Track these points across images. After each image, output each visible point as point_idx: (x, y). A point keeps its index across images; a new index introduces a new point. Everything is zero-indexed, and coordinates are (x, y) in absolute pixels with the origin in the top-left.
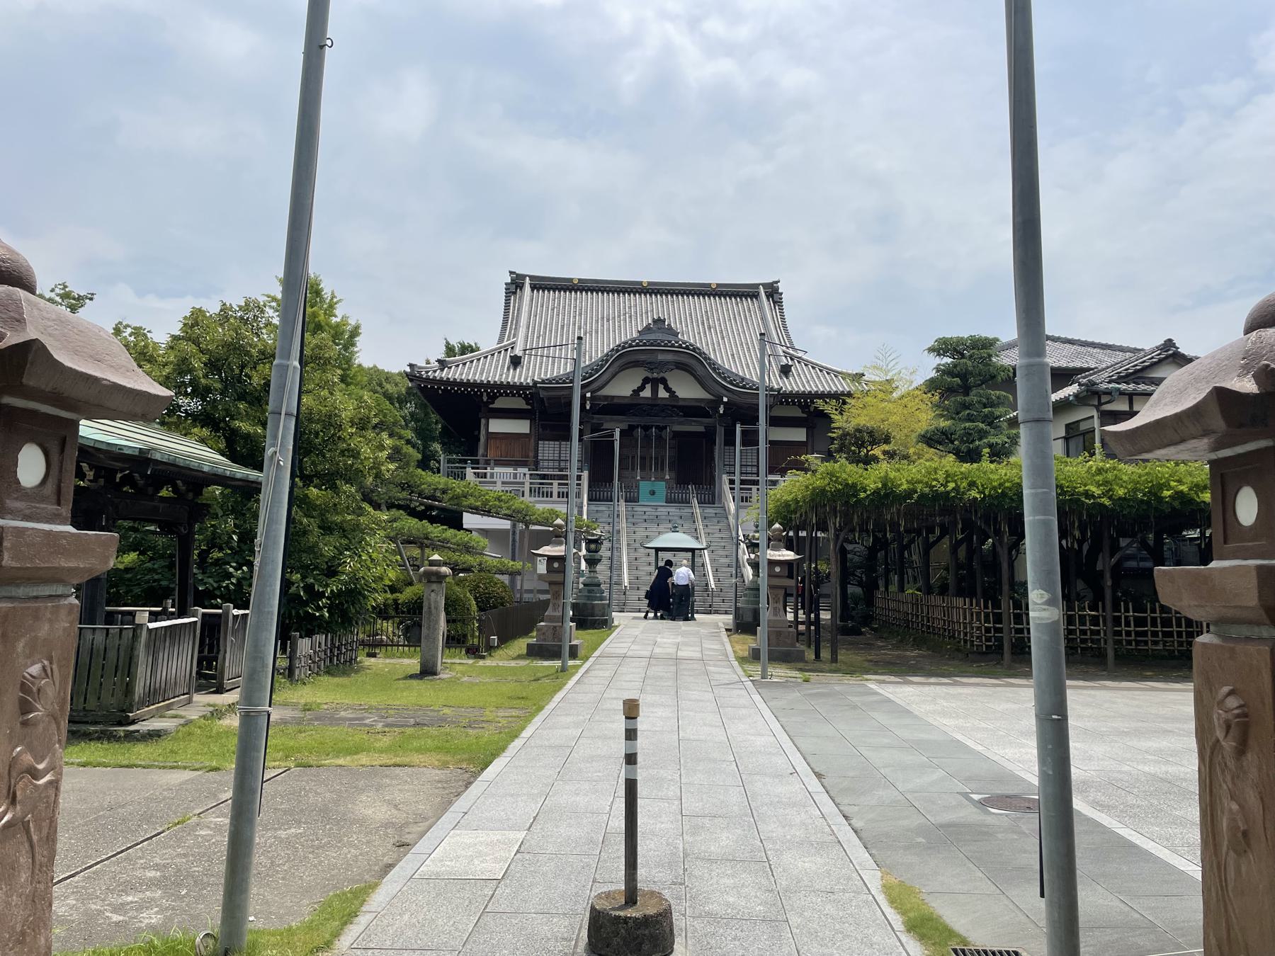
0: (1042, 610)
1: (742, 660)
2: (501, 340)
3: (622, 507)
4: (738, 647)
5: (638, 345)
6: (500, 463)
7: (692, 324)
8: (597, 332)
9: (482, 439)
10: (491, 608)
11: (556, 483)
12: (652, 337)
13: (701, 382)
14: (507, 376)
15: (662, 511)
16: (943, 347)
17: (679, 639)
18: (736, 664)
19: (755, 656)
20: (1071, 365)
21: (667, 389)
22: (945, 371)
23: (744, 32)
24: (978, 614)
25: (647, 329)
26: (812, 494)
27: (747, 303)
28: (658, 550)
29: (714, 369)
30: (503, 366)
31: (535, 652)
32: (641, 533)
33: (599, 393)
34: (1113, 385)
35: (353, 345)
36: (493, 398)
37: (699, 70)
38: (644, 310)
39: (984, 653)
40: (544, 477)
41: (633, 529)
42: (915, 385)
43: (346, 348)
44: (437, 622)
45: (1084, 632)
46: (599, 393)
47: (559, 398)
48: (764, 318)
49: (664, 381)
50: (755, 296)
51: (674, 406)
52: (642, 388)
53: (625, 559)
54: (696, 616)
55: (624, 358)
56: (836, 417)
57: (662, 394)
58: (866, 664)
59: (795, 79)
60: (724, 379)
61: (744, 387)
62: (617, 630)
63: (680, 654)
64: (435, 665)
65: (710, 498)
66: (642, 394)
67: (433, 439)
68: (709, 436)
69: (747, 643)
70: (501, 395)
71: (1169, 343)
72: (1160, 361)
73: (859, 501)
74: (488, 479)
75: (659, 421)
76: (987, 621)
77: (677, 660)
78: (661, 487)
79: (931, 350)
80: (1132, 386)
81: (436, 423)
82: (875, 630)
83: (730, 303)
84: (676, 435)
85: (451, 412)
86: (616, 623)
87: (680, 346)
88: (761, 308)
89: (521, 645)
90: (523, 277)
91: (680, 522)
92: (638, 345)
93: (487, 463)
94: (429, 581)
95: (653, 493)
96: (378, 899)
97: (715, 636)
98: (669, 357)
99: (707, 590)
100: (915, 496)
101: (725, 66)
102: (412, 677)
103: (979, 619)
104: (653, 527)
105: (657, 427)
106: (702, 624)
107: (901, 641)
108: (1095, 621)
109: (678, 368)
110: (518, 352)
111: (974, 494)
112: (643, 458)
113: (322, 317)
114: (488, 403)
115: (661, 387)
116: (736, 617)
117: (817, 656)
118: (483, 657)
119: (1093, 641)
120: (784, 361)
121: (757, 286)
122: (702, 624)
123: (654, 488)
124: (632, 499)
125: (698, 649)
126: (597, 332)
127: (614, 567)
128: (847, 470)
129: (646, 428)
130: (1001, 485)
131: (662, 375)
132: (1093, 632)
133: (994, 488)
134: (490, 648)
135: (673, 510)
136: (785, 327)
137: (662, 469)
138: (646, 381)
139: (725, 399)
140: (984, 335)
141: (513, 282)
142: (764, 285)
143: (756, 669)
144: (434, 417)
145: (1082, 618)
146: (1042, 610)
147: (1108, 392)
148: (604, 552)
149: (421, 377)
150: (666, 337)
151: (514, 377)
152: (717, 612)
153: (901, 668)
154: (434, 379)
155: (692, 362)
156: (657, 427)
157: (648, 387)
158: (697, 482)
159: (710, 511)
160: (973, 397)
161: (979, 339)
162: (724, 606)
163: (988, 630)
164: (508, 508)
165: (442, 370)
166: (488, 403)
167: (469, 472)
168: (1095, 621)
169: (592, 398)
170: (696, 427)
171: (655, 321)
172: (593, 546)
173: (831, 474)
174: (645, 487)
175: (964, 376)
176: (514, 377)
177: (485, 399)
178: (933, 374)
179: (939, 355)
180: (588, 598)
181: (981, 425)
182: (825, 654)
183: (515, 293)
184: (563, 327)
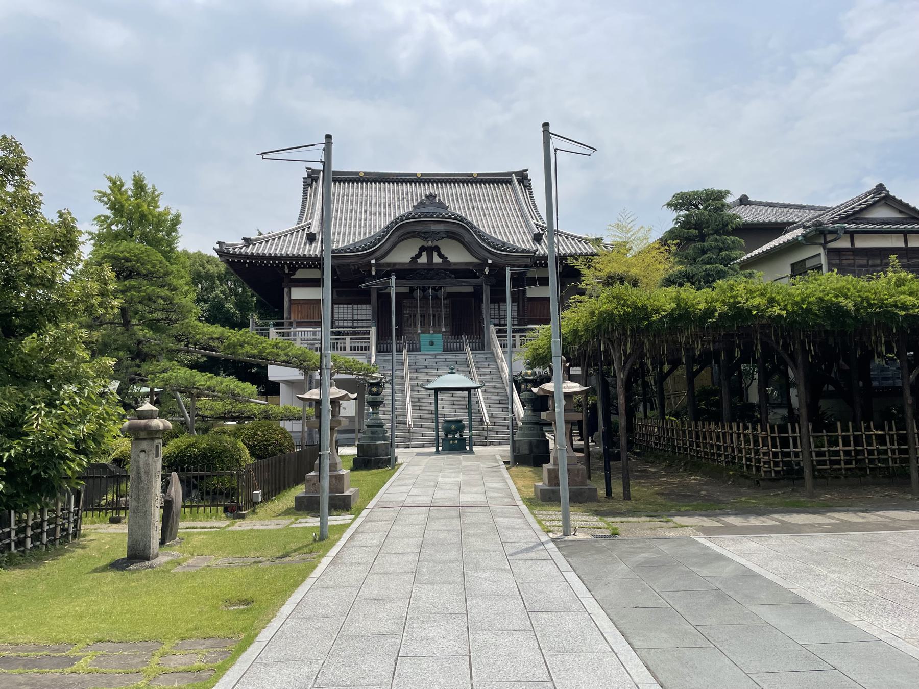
0: (852, 439)
1: (531, 503)
2: (300, 221)
3: (405, 355)
4: (520, 483)
5: (413, 218)
6: (300, 324)
7: (456, 201)
8: (380, 214)
9: (286, 305)
10: (270, 455)
11: (348, 338)
12: (425, 210)
14: (304, 250)
15: (440, 358)
16: (682, 201)
17: (460, 478)
18: (525, 509)
19: (548, 497)
20: (779, 220)
21: (440, 255)
22: (686, 224)
23: (485, 21)
24: (765, 439)
25: (421, 204)
26: (599, 319)
27: (503, 188)
28: (437, 390)
29: (479, 236)
30: (300, 243)
31: (307, 506)
32: (422, 377)
33: (384, 261)
34: (836, 225)
35: (175, 230)
36: (293, 270)
37: (453, 48)
38: (419, 192)
39: (771, 480)
40: (339, 333)
41: (416, 374)
42: (651, 241)
43: (169, 234)
44: (148, 490)
45: (871, 452)
46: (384, 261)
47: (348, 265)
48: (517, 199)
49: (437, 249)
50: (509, 182)
51: (445, 270)
52: (419, 255)
53: (408, 400)
54: (474, 448)
55: (403, 230)
56: (584, 271)
57: (437, 259)
58: (660, 499)
59: (523, 53)
60: (488, 244)
61: (505, 250)
62: (400, 470)
63: (465, 498)
64: (147, 546)
65: (481, 345)
66: (419, 261)
67: (250, 309)
68: (477, 295)
69: (533, 480)
70: (300, 267)
71: (880, 188)
72: (875, 203)
73: (650, 324)
74: (292, 337)
75: (433, 283)
76: (774, 446)
77: (460, 509)
78: (439, 338)
79: (669, 205)
80: (853, 226)
81: (253, 296)
82: (638, 454)
83: (489, 188)
84: (449, 295)
85: (262, 281)
86: (399, 461)
87: (450, 218)
88: (515, 192)
89: (288, 499)
91: (457, 366)
92: (413, 218)
93: (291, 324)
94: (137, 439)
95: (432, 344)
97: (495, 470)
98: (441, 227)
99: (482, 424)
100: (716, 314)
101: (473, 45)
102: (118, 565)
103: (765, 444)
104: (433, 372)
106: (480, 458)
107: (670, 466)
108: (881, 440)
109: (448, 237)
110: (314, 230)
111: (776, 310)
112: (423, 316)
113: (145, 207)
114: (289, 275)
115: (435, 254)
116: (514, 449)
117: (609, 492)
118: (242, 517)
119: (880, 461)
120: (536, 231)
121: (510, 174)
122: (480, 458)
123: (432, 339)
124: (414, 349)
125: (481, 489)
126: (380, 214)
127: (397, 407)
128: (718, 237)
129: (424, 290)
130: (803, 300)
131: (435, 243)
132: (880, 452)
133: (796, 303)
134: (252, 504)
135: (450, 357)
136: (535, 206)
137: (439, 325)
138: (422, 249)
139: (490, 262)
140: (716, 189)
141: (309, 176)
143: (553, 515)
144: (249, 291)
145: (869, 437)
146: (852, 439)
147: (833, 232)
148: (386, 393)
149: (228, 253)
150: (438, 211)
151: (310, 250)
152: (492, 444)
153: (710, 506)
154: (240, 254)
155: (460, 231)
156: (434, 289)
157: (424, 254)
158: (470, 334)
159: (481, 356)
160: (710, 242)
161: (713, 192)
162: (498, 438)
163: (775, 455)
164: (287, 355)
165: (248, 247)
166: (289, 275)
167: (273, 331)
168: (881, 440)
169: (376, 265)
170: (466, 288)
171: (427, 197)
172: (374, 389)
173: (618, 298)
174: (425, 339)
175: (698, 226)
176: (310, 250)
177: (287, 271)
178: (672, 225)
179: (676, 209)
180: (372, 439)
181: (721, 267)
182: (617, 489)
183: (311, 185)
184: (351, 210)
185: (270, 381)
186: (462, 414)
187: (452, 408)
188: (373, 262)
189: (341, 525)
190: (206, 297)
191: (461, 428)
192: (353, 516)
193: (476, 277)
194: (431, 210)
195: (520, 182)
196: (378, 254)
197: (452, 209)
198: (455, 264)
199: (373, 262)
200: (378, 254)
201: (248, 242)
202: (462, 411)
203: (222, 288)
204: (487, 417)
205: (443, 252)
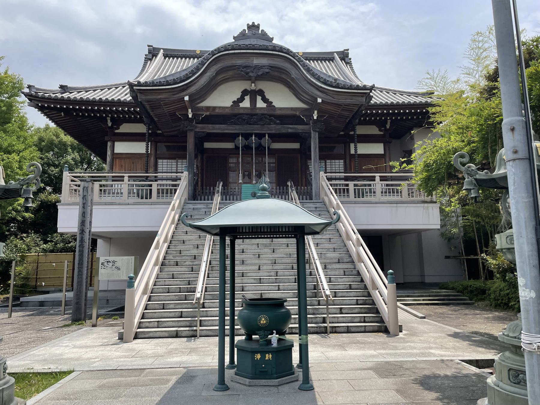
12: (247, 42)
13: (296, 92)
21: (265, 100)
25: (242, 35)
36: (117, 122)
49: (261, 93)
50: (332, 59)
51: (271, 116)
52: (241, 99)
66: (242, 105)
90: (159, 50)
96: (425, 91)
105: (257, 135)
115: (259, 98)
121: (332, 53)
138: (245, 93)
139: (319, 100)
142: (338, 53)
156: (257, 135)
157: (247, 98)
186: (288, 294)
187: (263, 271)
188: (187, 98)
190: (57, 163)
191: (279, 324)
193: (302, 122)
194: (253, 42)
195: (342, 59)
196: (193, 89)
197: (276, 41)
198: (281, 109)
199: (187, 98)
200: (193, 89)
201: (64, 88)
202: (287, 272)
203: (73, 156)
204: (326, 286)
205: (268, 96)
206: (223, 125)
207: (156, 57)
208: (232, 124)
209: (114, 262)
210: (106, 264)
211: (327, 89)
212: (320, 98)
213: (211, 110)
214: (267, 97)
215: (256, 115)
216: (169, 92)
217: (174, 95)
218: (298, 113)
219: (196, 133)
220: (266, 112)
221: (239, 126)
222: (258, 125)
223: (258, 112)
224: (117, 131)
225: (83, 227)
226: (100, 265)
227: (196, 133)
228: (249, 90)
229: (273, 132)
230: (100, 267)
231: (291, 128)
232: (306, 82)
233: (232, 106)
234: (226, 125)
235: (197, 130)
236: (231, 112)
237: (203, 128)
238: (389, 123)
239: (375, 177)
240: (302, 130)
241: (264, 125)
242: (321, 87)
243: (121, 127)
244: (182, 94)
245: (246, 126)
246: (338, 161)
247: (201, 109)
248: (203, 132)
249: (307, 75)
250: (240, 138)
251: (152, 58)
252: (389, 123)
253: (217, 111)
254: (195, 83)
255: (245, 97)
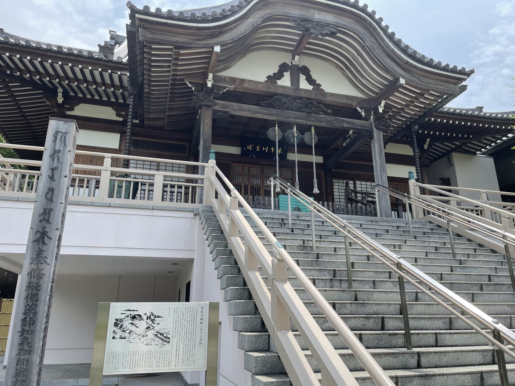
21: (310, 80)
36: (72, 101)
49: (305, 71)
52: (279, 75)
66: (279, 82)
115: (303, 78)
138: (284, 68)
157: (287, 75)
185: (190, 385)
188: (217, 49)
189: (265, 120)
192: (388, 187)
196: (227, 37)
198: (332, 95)
199: (217, 49)
200: (227, 37)
206: (255, 107)
207: (120, 45)
208: (266, 107)
209: (152, 318)
210: (127, 323)
211: (415, 67)
212: (404, 77)
213: (237, 82)
214: (314, 77)
215: (301, 98)
216: (190, 35)
217: (198, 40)
218: (354, 104)
219: (215, 112)
220: (313, 97)
221: (277, 110)
222: (302, 112)
223: (302, 94)
224: (69, 113)
225: (44, 223)
226: (111, 327)
227: (215, 112)
228: (290, 65)
229: (324, 124)
230: (110, 335)
231: (346, 122)
232: (384, 55)
233: (266, 81)
234: (258, 107)
235: (217, 108)
236: (266, 89)
237: (224, 106)
238: (427, 143)
239: (480, 193)
240: (362, 126)
241: (310, 113)
242: (407, 63)
243: (76, 108)
244: (211, 41)
245: (286, 111)
246: (364, 183)
247: (224, 79)
248: (225, 112)
249: (390, 44)
250: (277, 128)
251: (115, 46)
252: (427, 143)
253: (246, 85)
254: (231, 30)
255: (284, 73)
